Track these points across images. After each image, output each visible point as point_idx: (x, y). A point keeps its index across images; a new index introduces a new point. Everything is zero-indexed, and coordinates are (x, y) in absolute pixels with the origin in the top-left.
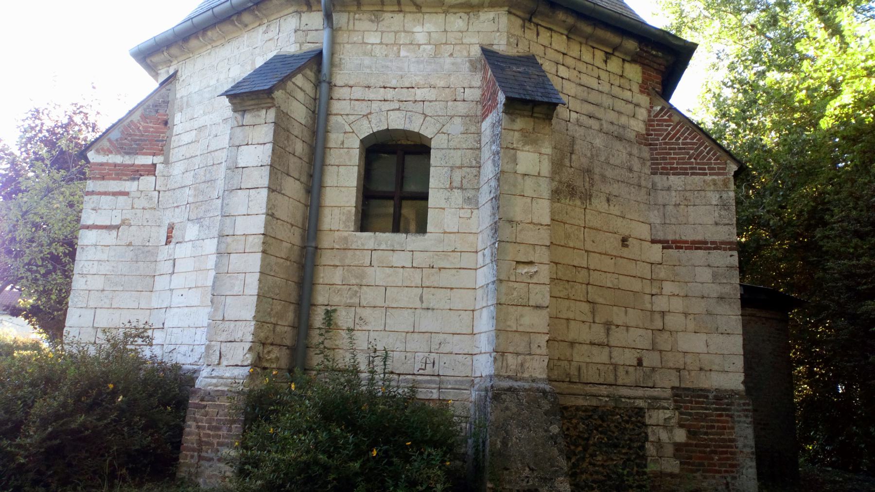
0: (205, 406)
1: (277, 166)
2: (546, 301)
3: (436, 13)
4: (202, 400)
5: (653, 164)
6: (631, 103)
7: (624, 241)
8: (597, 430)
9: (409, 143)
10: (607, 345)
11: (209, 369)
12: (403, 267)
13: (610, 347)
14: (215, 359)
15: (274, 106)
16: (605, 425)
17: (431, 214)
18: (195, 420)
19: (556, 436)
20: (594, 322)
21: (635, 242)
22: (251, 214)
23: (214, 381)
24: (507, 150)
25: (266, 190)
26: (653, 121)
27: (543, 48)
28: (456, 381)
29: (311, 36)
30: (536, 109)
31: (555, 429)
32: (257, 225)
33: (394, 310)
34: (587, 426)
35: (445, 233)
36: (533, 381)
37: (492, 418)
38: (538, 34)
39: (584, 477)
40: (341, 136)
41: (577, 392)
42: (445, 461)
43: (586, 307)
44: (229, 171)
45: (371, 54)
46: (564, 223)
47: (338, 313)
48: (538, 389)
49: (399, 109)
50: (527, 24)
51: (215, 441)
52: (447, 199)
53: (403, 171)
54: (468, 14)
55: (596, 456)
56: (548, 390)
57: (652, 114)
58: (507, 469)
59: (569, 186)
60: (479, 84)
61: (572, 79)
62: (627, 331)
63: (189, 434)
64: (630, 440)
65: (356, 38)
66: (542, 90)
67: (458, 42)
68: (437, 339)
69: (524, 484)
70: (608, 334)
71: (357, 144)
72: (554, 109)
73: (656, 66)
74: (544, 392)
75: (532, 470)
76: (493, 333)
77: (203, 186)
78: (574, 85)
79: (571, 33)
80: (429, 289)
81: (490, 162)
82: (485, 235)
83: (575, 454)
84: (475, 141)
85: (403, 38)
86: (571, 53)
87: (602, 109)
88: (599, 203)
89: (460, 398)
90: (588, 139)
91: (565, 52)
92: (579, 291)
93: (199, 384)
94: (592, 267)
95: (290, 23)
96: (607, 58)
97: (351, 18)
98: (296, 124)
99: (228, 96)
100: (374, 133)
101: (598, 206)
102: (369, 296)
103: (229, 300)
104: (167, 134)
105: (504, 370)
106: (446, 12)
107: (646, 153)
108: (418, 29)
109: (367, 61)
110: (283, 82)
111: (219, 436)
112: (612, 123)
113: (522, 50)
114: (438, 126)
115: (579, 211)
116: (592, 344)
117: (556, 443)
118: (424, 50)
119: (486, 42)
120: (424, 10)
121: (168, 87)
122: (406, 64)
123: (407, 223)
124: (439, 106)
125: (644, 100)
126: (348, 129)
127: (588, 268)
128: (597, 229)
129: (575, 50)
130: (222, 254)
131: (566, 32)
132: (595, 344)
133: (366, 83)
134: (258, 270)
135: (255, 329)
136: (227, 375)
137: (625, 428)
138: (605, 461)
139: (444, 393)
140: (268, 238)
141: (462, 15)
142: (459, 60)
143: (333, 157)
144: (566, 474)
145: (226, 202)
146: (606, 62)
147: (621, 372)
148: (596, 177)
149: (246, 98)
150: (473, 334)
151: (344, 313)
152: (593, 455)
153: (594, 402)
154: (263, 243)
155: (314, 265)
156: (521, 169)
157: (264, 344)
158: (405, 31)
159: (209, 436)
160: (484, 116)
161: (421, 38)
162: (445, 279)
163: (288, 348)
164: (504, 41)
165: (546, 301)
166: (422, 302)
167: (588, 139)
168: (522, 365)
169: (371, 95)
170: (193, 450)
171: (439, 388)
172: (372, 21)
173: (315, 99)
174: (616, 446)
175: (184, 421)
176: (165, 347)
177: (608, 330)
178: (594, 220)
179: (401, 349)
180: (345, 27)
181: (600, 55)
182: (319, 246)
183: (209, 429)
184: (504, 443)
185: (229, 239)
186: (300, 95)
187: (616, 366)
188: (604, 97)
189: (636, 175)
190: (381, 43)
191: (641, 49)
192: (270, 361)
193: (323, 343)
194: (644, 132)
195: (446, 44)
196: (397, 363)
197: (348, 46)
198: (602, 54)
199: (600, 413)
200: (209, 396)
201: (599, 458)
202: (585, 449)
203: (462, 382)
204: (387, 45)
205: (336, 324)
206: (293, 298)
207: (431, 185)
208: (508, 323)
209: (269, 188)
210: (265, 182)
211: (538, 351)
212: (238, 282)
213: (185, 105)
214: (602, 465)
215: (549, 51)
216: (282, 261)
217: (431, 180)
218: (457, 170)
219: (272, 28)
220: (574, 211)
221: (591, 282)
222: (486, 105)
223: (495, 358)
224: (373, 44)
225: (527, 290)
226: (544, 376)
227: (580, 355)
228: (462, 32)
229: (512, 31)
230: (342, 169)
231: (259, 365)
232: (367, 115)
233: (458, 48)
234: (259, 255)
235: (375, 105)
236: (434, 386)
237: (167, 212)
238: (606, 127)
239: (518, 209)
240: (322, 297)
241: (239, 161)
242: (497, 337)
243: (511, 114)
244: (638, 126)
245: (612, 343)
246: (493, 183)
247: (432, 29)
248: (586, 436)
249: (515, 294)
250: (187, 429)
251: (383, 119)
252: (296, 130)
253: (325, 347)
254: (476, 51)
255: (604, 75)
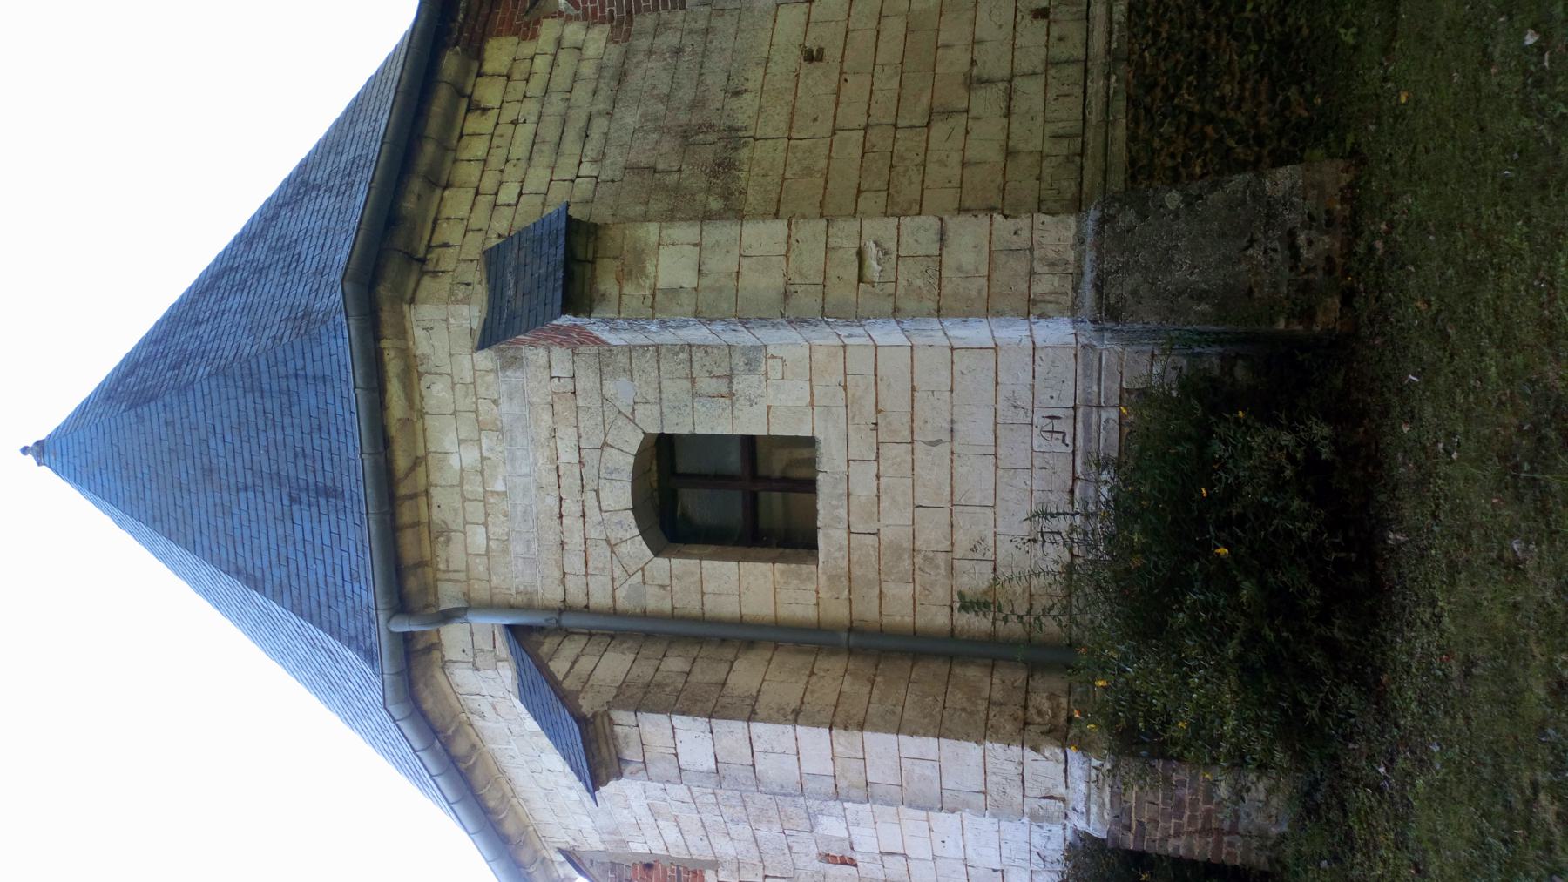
0: (1140, 823)
1: (711, 705)
2: (930, 222)
3: (424, 430)
4: (1129, 828)
5: (665, 7)
6: (555, 55)
7: (812, 56)
8: (1172, 97)
9: (654, 468)
10: (1010, 81)
11: (1073, 817)
12: (878, 477)
13: (1013, 76)
14: (1055, 807)
15: (606, 713)
16: (1163, 81)
17: (778, 430)
18: (1165, 839)
19: (1186, 196)
20: (967, 111)
21: (812, 35)
22: (797, 750)
23: (1094, 809)
24: (658, 306)
25: (753, 725)
26: (585, 9)
27: (470, 235)
28: (1085, 376)
29: (483, 642)
30: (580, 255)
31: (1173, 199)
32: (815, 744)
33: (956, 491)
34: (1165, 117)
35: (812, 405)
36: (1081, 241)
37: (1153, 322)
38: (446, 245)
39: (1264, 120)
40: (651, 590)
41: (1100, 139)
42: (1237, 419)
43: (939, 129)
44: (724, 785)
45: (506, 542)
46: (784, 179)
47: (965, 589)
48: (1098, 234)
49: (597, 492)
50: (430, 267)
51: (1202, 807)
52: (751, 402)
53: (706, 476)
54: (420, 375)
55: (1223, 97)
56: (1099, 214)
57: (574, 12)
58: (1251, 291)
59: (714, 174)
60: (542, 352)
61: (520, 175)
62: (981, 42)
63: (1190, 849)
64: (1190, 27)
65: (480, 567)
66: (545, 244)
67: (471, 390)
68: (1006, 413)
69: (1278, 257)
70: (989, 82)
71: (662, 562)
72: (578, 221)
73: (485, 10)
74: (1102, 221)
75: (1251, 243)
76: (994, 321)
77: (751, 809)
78: (531, 170)
79: (438, 182)
80: (916, 430)
81: (679, 332)
82: (814, 335)
83: (1221, 140)
84: (644, 354)
85: (473, 487)
86: (474, 180)
87: (571, 113)
88: (744, 111)
89: (1115, 368)
90: (627, 138)
91: (473, 191)
92: (908, 143)
93: (1098, 830)
94: (863, 121)
95: (463, 677)
96: (478, 108)
97: (446, 576)
98: (636, 670)
99: (596, 788)
100: (642, 533)
101: (749, 112)
102: (932, 535)
103: (948, 784)
104: (667, 864)
105: (1062, 299)
106: (422, 414)
107: (646, 21)
108: (454, 461)
109: (518, 548)
110: (566, 698)
111: (1194, 803)
112: (595, 92)
113: (475, 275)
114: (621, 422)
115: (761, 151)
116: (1008, 113)
117: (1200, 197)
118: (491, 449)
119: (468, 343)
120: (421, 453)
121: (588, 865)
122: (518, 480)
123: (794, 463)
124: (586, 422)
125: (548, 30)
126: (637, 578)
127: (865, 129)
128: (792, 114)
129: (467, 172)
130: (868, 794)
131: (438, 191)
132: (1009, 108)
133: (556, 549)
134: (894, 737)
135: (999, 740)
136: (1083, 787)
137: (1168, 39)
138: (1233, 76)
139: (1107, 399)
140: (838, 720)
141: (423, 384)
142: (504, 387)
143: (689, 603)
144: (1260, 175)
145: (777, 790)
146: (485, 110)
147: (1061, 52)
148: (696, 119)
149: (597, 760)
150: (996, 348)
151: (965, 579)
152: (1222, 103)
153: (1120, 104)
154: (846, 728)
155: (881, 632)
156: (688, 279)
157: (1026, 723)
158: (461, 484)
159: (1192, 818)
160: (598, 341)
161: (470, 456)
162: (895, 401)
163: (1030, 675)
164: (464, 310)
165: (930, 222)
166: (940, 441)
167: (627, 138)
168: (1052, 264)
169: (575, 541)
170: (1218, 843)
171: (1099, 406)
172: (448, 540)
173: (591, 635)
174: (1204, 57)
175: (1167, 857)
176: (1034, 868)
177: (981, 81)
178: (776, 122)
179: (1027, 478)
180: (464, 587)
181: (474, 123)
182: (847, 623)
183: (1181, 817)
184: (1201, 296)
185: (842, 783)
186: (585, 664)
187: (1050, 63)
188: (549, 110)
189: (687, 40)
190: (485, 524)
191: (457, 44)
192: (1055, 710)
193: (1020, 618)
194: (607, 27)
195: (476, 412)
196: (1052, 488)
197: (495, 581)
198: (471, 117)
199: (1141, 92)
200: (1121, 816)
201: (1227, 89)
202: (1210, 119)
203: (1087, 366)
204: (487, 515)
205: (985, 593)
206: (940, 668)
207: (727, 431)
208: (974, 293)
209: (749, 720)
210: (739, 726)
211: (1025, 234)
212: (917, 770)
213: (617, 838)
214: (1242, 82)
215: (475, 223)
216: (875, 691)
217: (718, 431)
218: (698, 385)
219: (474, 706)
220: (761, 162)
221: (892, 120)
222: (576, 341)
223: (1040, 316)
224: (488, 539)
225: (910, 262)
226: (1072, 220)
227: (1030, 137)
228: (454, 384)
229: (445, 294)
230: (709, 587)
231: (1061, 734)
232: (612, 547)
233: (482, 391)
234: (867, 735)
235: (593, 533)
236: (1094, 417)
237: (801, 862)
238: (602, 105)
239: (763, 282)
240: (937, 617)
241: (705, 768)
242: (999, 314)
243: (592, 300)
244: (596, 40)
245: (1006, 73)
246: (718, 327)
247: (453, 436)
248: (1185, 120)
249: (919, 282)
250: (1182, 852)
251: (615, 519)
252: (645, 670)
253: (1029, 613)
254: (485, 359)
255: (510, 113)
